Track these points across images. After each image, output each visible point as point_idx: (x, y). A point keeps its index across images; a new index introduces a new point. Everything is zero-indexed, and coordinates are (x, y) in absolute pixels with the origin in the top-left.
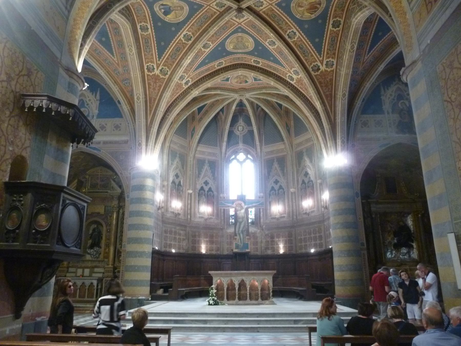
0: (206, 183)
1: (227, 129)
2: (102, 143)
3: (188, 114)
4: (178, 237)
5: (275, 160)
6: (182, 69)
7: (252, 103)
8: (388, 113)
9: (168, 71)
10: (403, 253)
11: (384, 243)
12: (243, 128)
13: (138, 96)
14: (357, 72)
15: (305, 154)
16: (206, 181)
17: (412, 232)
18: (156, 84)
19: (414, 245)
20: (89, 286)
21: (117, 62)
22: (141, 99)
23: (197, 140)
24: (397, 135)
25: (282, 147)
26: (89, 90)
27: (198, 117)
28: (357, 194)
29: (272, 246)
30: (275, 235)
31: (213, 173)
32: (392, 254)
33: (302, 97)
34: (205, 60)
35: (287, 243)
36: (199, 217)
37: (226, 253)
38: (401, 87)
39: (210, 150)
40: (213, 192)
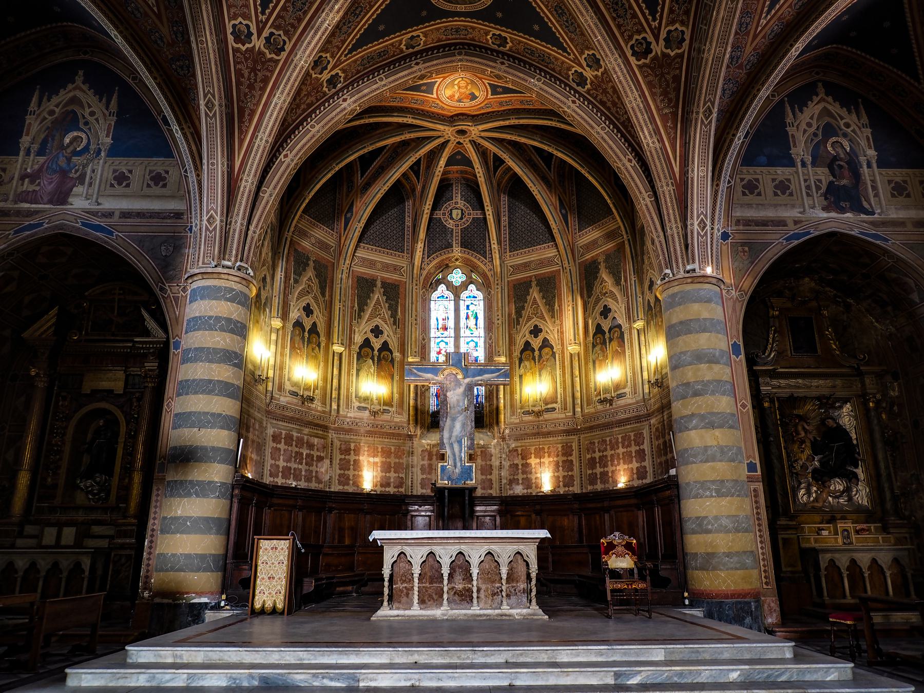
0: (377, 331)
1: (426, 211)
2: (117, 214)
3: (337, 169)
4: (305, 452)
5: (534, 284)
6: (321, 38)
7: (483, 153)
8: (804, 164)
9: (285, 42)
10: (835, 491)
11: (791, 466)
12: (462, 214)
13: (209, 100)
14: (738, 58)
15: (602, 267)
16: (377, 326)
17: (855, 442)
18: (256, 75)
19: (860, 472)
20: (26, 571)
21: (155, 9)
22: (217, 108)
23: (357, 234)
24: (825, 215)
25: (550, 253)
26: (92, 91)
27: (359, 180)
28: (735, 347)
29: (525, 476)
30: (533, 452)
31: (393, 310)
32: (809, 493)
33: (604, 125)
34: (376, 22)
35: (561, 468)
36: (359, 408)
37: (419, 491)
38: (830, 107)
39: (387, 260)
40: (392, 353)
